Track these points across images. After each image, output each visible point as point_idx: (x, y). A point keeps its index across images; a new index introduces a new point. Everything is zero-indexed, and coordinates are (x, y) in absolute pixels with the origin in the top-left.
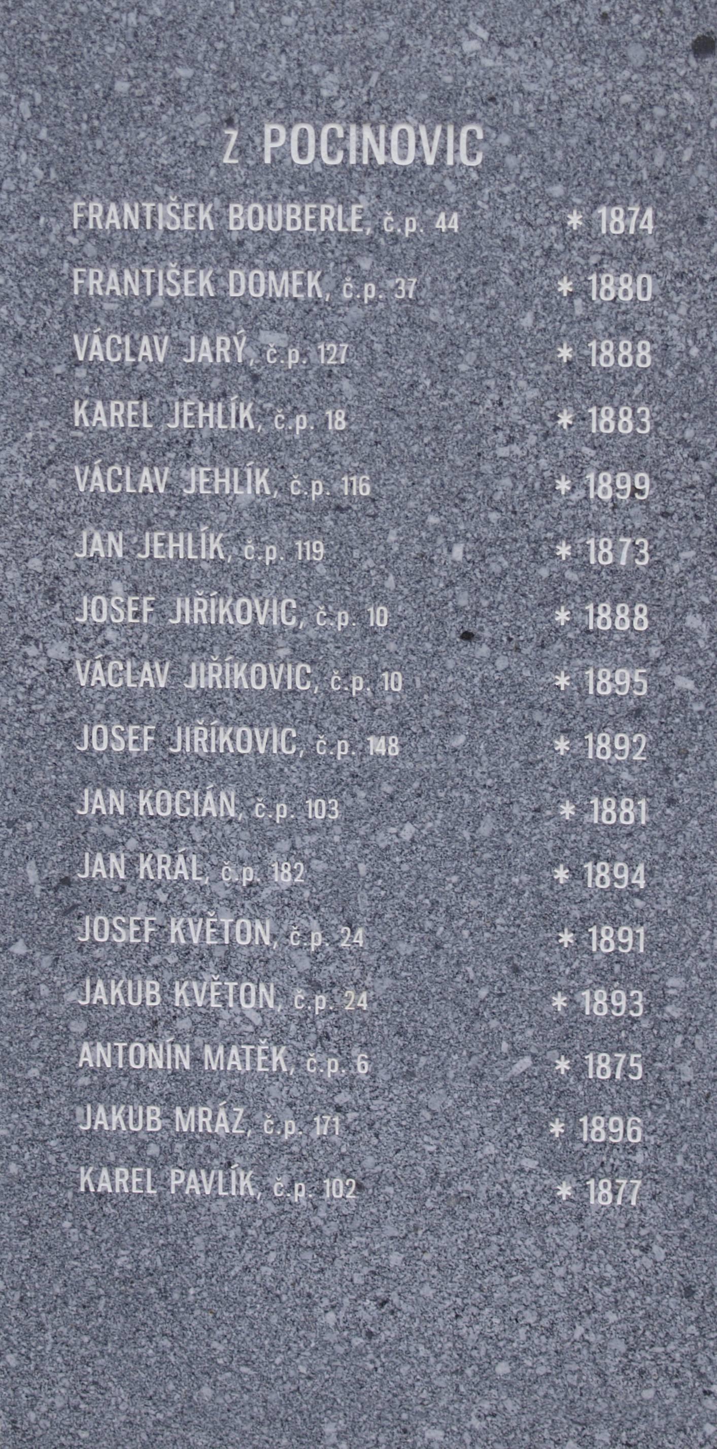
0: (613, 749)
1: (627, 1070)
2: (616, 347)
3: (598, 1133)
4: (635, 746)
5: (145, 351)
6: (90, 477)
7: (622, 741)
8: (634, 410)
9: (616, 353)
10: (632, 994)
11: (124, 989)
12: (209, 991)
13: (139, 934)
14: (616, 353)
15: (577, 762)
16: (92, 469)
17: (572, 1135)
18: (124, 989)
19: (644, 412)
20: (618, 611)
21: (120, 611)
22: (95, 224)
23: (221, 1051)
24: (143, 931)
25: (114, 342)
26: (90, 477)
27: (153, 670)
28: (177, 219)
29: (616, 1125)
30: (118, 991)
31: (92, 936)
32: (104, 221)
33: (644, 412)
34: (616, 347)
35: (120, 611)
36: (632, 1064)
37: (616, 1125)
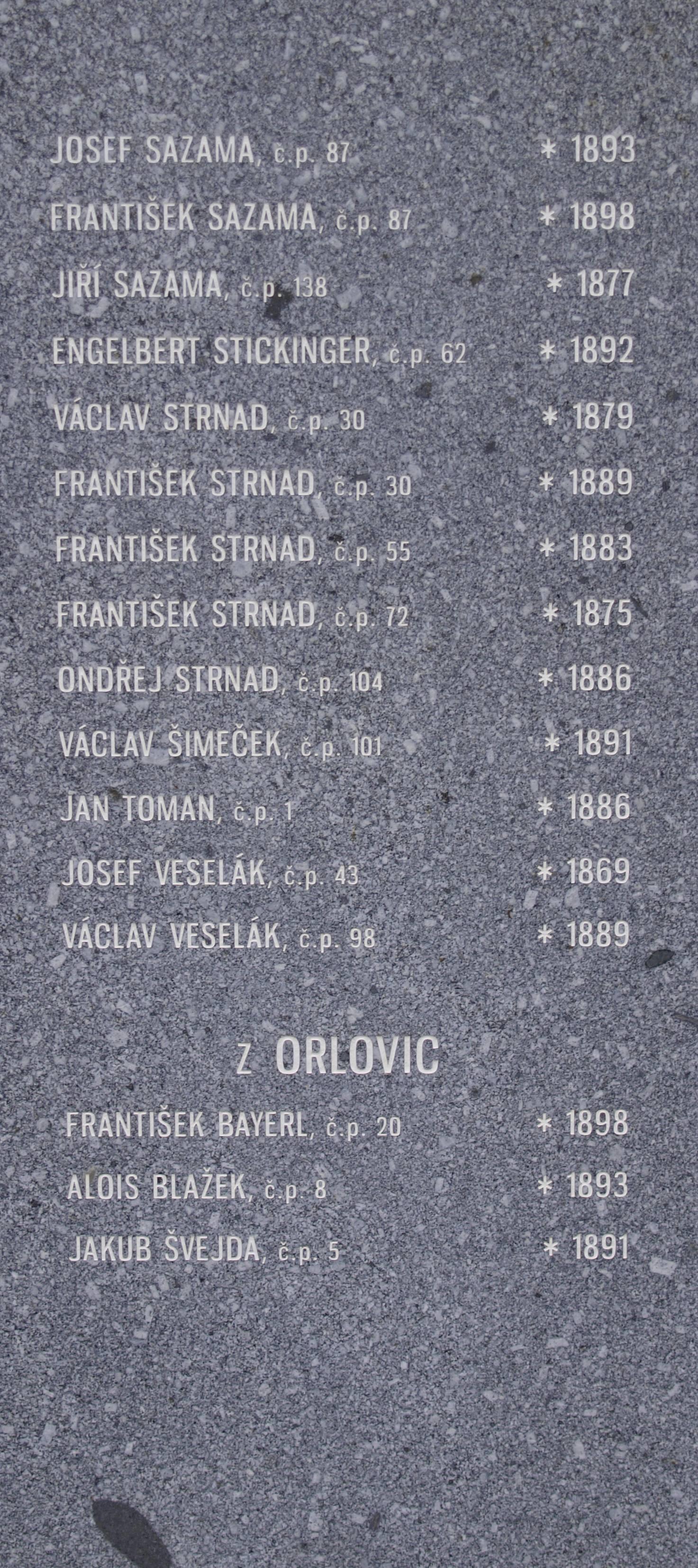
0: (601, 150)
1: (614, 615)
2: (598, 540)
3: (588, 485)
4: (622, 348)
5: (133, 939)
6: (70, 414)
7: (608, 345)
8: (615, 538)
9: (598, 547)
10: (621, 537)
11: (115, 1244)
12: (195, 1245)
13: (115, 155)
14: (598, 547)
15: (560, 560)
16: (79, 927)
17: (560, 815)
18: (115, 1244)
19: (625, 539)
20: (600, 802)
21: (96, 150)
22: (79, 622)
23: (200, 275)
24: (118, 152)
25: (99, 738)
26: (70, 414)
27: (140, 932)
28: (160, 551)
29: (608, 211)
30: (109, 1247)
31: (76, 880)
32: (88, 619)
33: (625, 539)
34: (598, 540)
35: (96, 150)
36: (621, 610)
37: (608, 211)
